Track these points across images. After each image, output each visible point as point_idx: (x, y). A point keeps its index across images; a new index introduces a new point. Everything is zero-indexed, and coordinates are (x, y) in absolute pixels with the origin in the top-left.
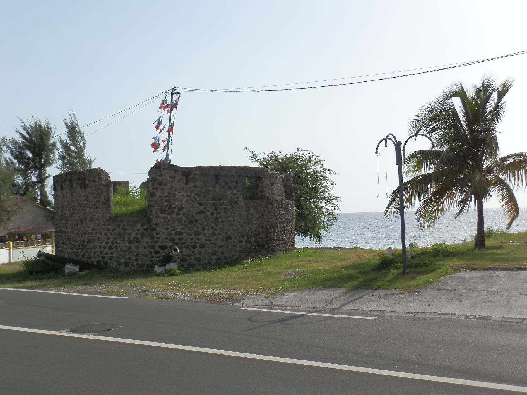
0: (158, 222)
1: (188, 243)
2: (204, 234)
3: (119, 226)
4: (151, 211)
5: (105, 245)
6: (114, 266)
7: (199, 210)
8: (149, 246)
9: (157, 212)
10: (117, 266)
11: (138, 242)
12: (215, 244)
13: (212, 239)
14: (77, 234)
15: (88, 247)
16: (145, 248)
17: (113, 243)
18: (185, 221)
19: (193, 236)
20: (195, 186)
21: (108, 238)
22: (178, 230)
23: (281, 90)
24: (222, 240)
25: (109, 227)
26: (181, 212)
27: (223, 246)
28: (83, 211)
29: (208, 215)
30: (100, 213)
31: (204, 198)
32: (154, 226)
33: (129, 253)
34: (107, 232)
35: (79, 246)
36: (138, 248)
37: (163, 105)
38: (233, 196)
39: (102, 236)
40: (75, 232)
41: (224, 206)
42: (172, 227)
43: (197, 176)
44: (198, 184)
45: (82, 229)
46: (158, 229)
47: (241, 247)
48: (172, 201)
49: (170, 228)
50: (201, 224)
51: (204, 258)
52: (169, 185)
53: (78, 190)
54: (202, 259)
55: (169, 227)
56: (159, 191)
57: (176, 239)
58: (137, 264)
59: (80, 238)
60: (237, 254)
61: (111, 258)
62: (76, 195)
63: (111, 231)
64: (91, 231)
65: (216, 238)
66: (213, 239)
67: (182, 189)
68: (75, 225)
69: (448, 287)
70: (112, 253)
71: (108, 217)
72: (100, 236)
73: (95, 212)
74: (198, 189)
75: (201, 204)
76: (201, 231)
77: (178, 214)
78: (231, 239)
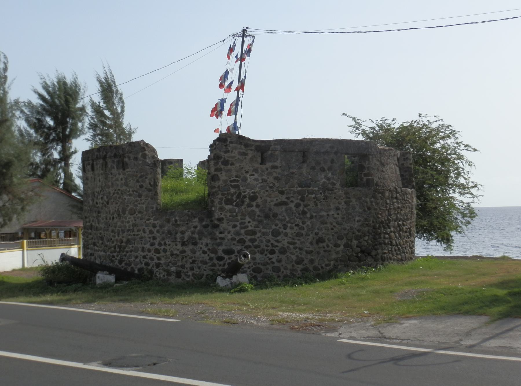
0: (222, 216)
2: (286, 235)
3: (168, 221)
4: (212, 202)
7: (279, 200)
8: (209, 249)
9: (220, 203)
10: (166, 277)
11: (195, 244)
12: (301, 249)
14: (113, 231)
15: (127, 249)
16: (204, 252)
17: (160, 244)
18: (259, 216)
20: (275, 167)
21: (154, 238)
22: (250, 228)
23: (398, 30)
25: (156, 222)
26: (254, 204)
27: (312, 251)
30: (143, 203)
32: (216, 222)
33: (183, 258)
34: (153, 229)
36: (194, 252)
39: (146, 235)
40: (110, 229)
41: (313, 196)
42: (241, 223)
43: (277, 153)
44: (278, 163)
46: (223, 226)
47: (337, 253)
48: (241, 188)
49: (239, 226)
51: (286, 268)
53: (114, 171)
54: (282, 269)
55: (238, 224)
56: (224, 173)
57: (247, 240)
58: (193, 275)
59: (117, 237)
60: (332, 263)
61: (158, 265)
62: (112, 178)
63: (158, 228)
64: (131, 228)
65: (303, 240)
67: (256, 170)
70: (159, 259)
71: (155, 209)
72: (143, 235)
73: (137, 201)
74: (278, 170)
75: (282, 193)
76: (281, 230)
77: (249, 205)
78: (324, 241)
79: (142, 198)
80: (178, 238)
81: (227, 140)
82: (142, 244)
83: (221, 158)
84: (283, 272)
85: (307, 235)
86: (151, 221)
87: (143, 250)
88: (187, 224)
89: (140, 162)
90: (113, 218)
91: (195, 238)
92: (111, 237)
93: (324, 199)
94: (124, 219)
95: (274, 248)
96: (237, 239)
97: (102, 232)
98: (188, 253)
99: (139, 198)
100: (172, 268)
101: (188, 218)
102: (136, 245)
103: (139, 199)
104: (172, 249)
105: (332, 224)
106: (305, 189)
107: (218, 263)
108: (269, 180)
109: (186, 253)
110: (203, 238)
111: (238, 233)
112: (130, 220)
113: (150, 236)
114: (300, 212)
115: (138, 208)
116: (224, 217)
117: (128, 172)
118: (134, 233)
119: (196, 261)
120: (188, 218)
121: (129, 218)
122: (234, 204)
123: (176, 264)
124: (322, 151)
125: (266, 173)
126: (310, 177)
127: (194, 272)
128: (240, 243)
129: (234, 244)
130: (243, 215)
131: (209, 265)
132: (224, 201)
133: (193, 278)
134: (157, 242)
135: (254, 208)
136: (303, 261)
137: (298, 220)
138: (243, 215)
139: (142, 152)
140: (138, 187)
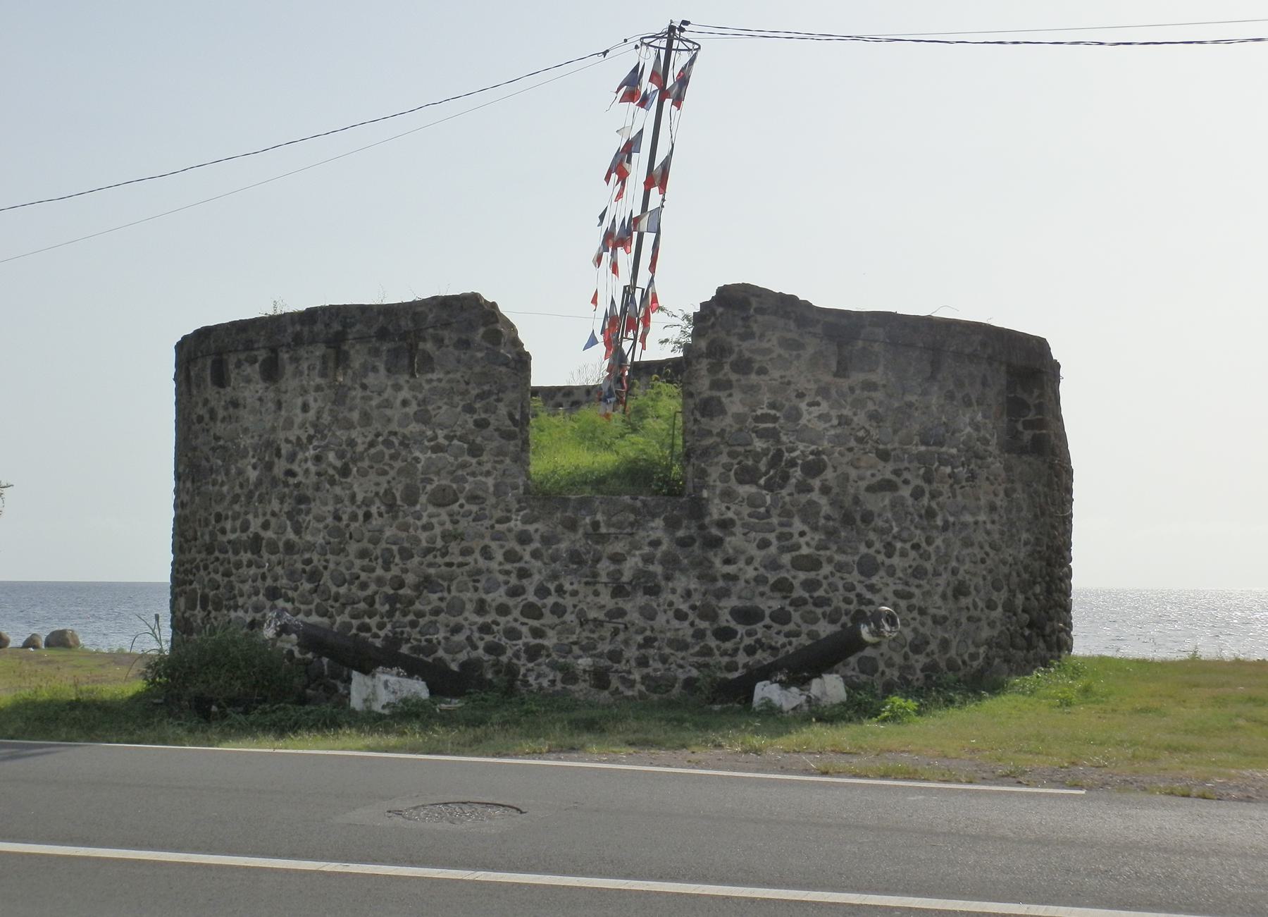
0: (730, 515)
1: (838, 602)
2: (891, 571)
3: (572, 525)
4: (703, 474)
5: (505, 599)
6: (545, 683)
7: (879, 477)
8: (693, 608)
9: (724, 478)
10: (559, 686)
11: (653, 591)
12: (922, 612)
13: (913, 590)
14: (363, 554)
15: (418, 606)
16: (680, 616)
17: (542, 591)
18: (828, 518)
19: (855, 577)
20: (870, 386)
21: (524, 574)
22: (805, 551)
23: (1229, 42)
24: (944, 596)
25: (531, 528)
26: (816, 483)
27: (945, 618)
28: (398, 464)
29: (902, 498)
30: (488, 474)
31: (895, 432)
32: (715, 531)
33: (616, 632)
34: (518, 548)
35: (371, 601)
36: (649, 614)
37: (631, 90)
38: (975, 435)
39: (494, 565)
40: (353, 548)
41: (948, 470)
42: (781, 537)
43: (877, 347)
44: (877, 377)
45: (388, 533)
46: (734, 541)
47: (992, 624)
48: (784, 438)
49: (774, 542)
50: (881, 532)
51: (890, 664)
52: (776, 374)
53: (376, 379)
54: (882, 667)
55: (772, 537)
56: (738, 396)
57: (796, 583)
58: (645, 678)
59: (379, 572)
60: (982, 650)
61: (533, 653)
62: (366, 399)
63: (536, 545)
64: (439, 543)
65: (927, 587)
66: (916, 591)
67: (824, 391)
68: (354, 517)
70: (537, 633)
71: (521, 491)
72: (482, 563)
73: (464, 466)
74: (879, 395)
75: (884, 456)
76: (881, 558)
77: (804, 488)
78: (966, 594)
79: (484, 458)
81: (750, 304)
82: (476, 589)
83: (731, 351)
84: (883, 673)
85: (937, 574)
86: (512, 524)
87: (481, 608)
88: (631, 534)
89: (479, 355)
90: (368, 516)
91: (653, 575)
92: (356, 570)
93: (967, 480)
94: (410, 520)
95: (863, 608)
96: (771, 581)
97: (315, 557)
98: (634, 616)
99: (474, 456)
100: (580, 661)
101: (632, 517)
102: (454, 593)
103: (474, 461)
104: (583, 606)
105: (982, 548)
106: (933, 448)
107: (719, 648)
108: (855, 419)
109: (627, 618)
110: (677, 574)
111: (774, 565)
112: (434, 520)
113: (508, 567)
114: (923, 512)
115: (467, 486)
116: (735, 517)
117: (429, 381)
118: (447, 559)
119: (655, 639)
120: (632, 517)
121: (430, 516)
122: (762, 481)
123: (595, 648)
124: (967, 351)
125: (849, 400)
126: (944, 419)
127: (650, 670)
128: (780, 590)
129: (762, 594)
130: (786, 513)
131: (692, 651)
132: (736, 474)
133: (643, 688)
134: (531, 585)
135: (815, 496)
136: (928, 643)
137: (918, 532)
138: (786, 513)
139: (485, 325)
140: (471, 425)
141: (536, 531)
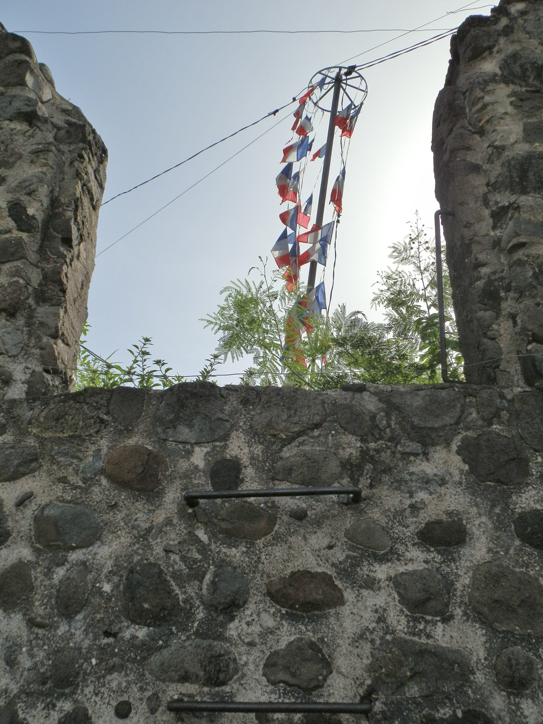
69: (334, 497)
80: (252, 662)
91: (450, 667)
101: (351, 446)
120: (351, 446)
141: (22, 502)
